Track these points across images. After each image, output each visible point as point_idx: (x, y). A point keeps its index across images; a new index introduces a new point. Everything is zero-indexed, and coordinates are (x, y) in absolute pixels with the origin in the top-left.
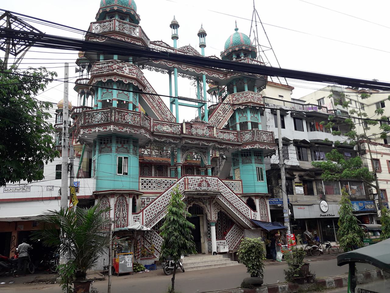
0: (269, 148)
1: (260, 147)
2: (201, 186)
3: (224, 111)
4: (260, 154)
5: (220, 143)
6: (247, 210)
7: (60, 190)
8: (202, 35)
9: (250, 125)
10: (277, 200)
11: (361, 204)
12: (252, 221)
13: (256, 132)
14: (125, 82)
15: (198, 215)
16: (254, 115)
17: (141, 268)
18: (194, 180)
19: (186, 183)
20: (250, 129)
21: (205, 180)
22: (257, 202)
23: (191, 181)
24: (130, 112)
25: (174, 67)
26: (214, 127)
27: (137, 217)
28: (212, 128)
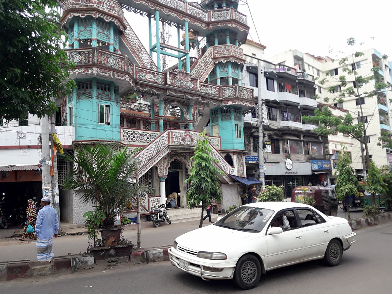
0: (249, 105)
1: (241, 103)
2: (185, 140)
3: (205, 64)
4: (239, 111)
5: (203, 97)
6: (225, 165)
7: (40, 137)
9: (230, 81)
10: (249, 157)
11: (320, 163)
12: (231, 177)
13: (238, 87)
14: (106, 20)
15: (177, 170)
16: (235, 71)
17: (127, 221)
18: (178, 134)
19: (171, 136)
20: (230, 85)
22: (235, 158)
23: (175, 135)
25: (155, 10)
26: (197, 80)
28: (196, 81)
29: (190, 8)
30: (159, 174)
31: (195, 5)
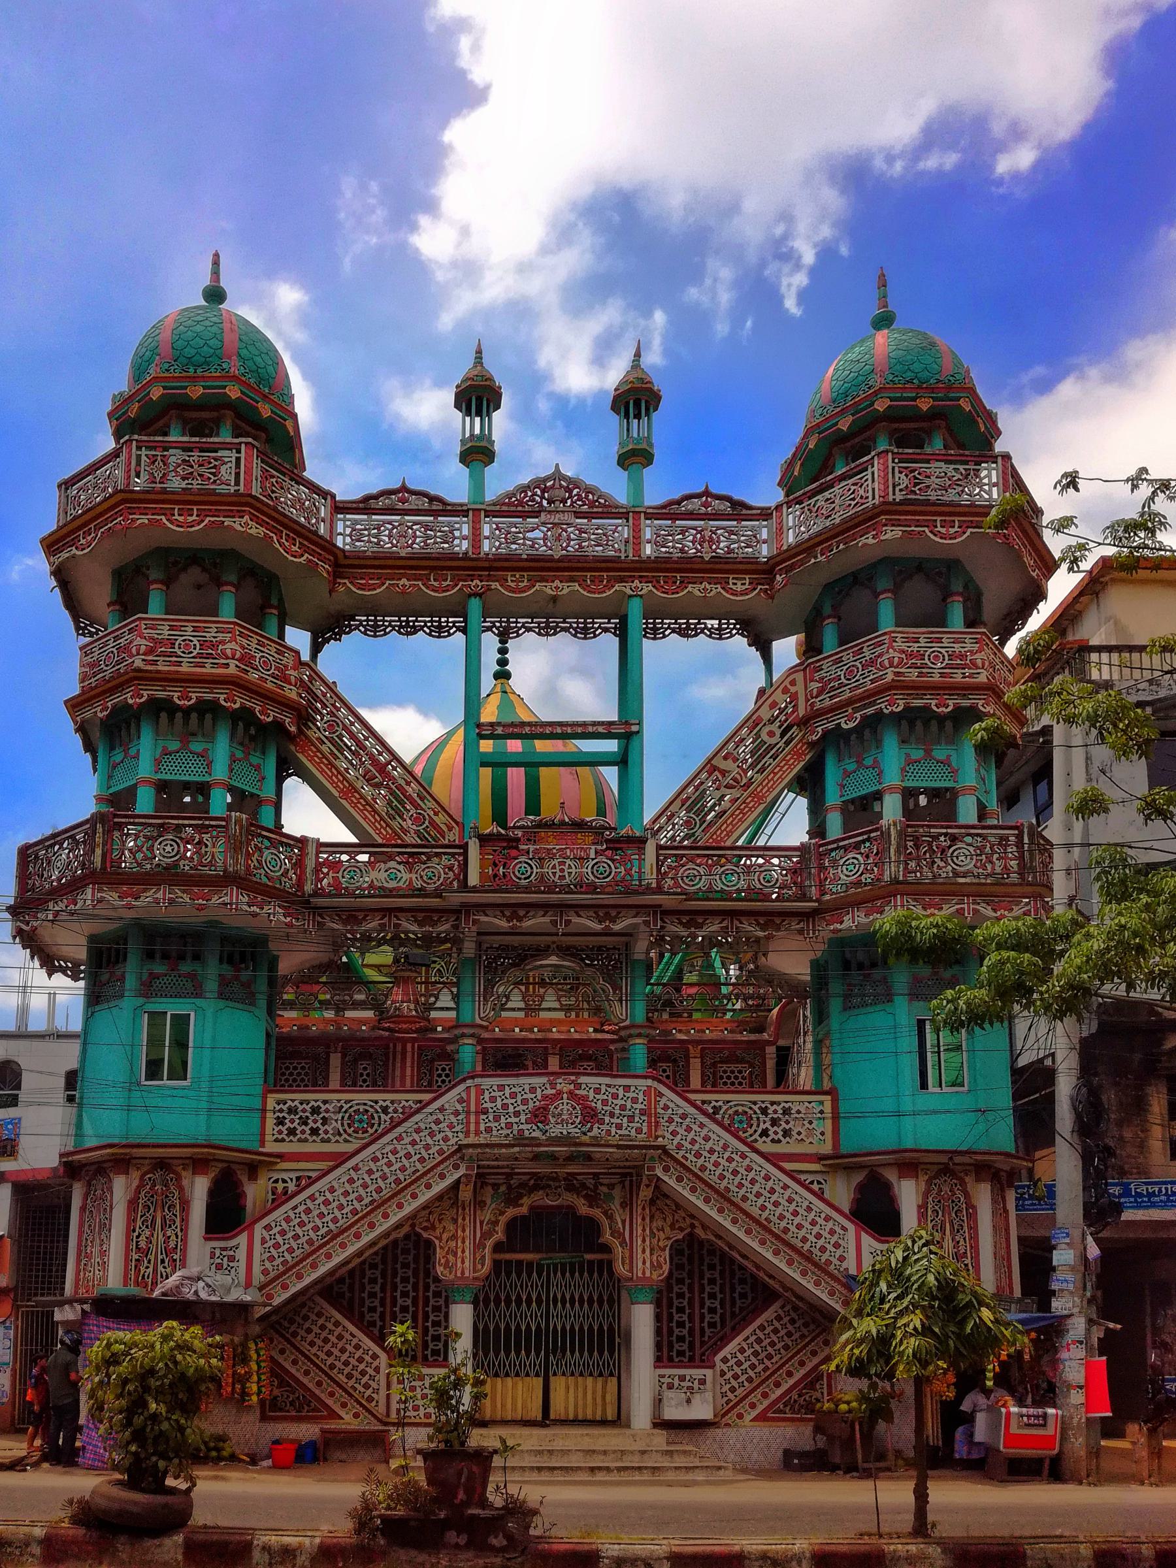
2: (545, 1122)
8: (485, 403)
18: (513, 1095)
19: (473, 1109)
21: (570, 1093)
23: (493, 1099)
24: (186, 822)
27: (224, 1253)
29: (660, 528)
30: (440, 1270)
31: (694, 505)
